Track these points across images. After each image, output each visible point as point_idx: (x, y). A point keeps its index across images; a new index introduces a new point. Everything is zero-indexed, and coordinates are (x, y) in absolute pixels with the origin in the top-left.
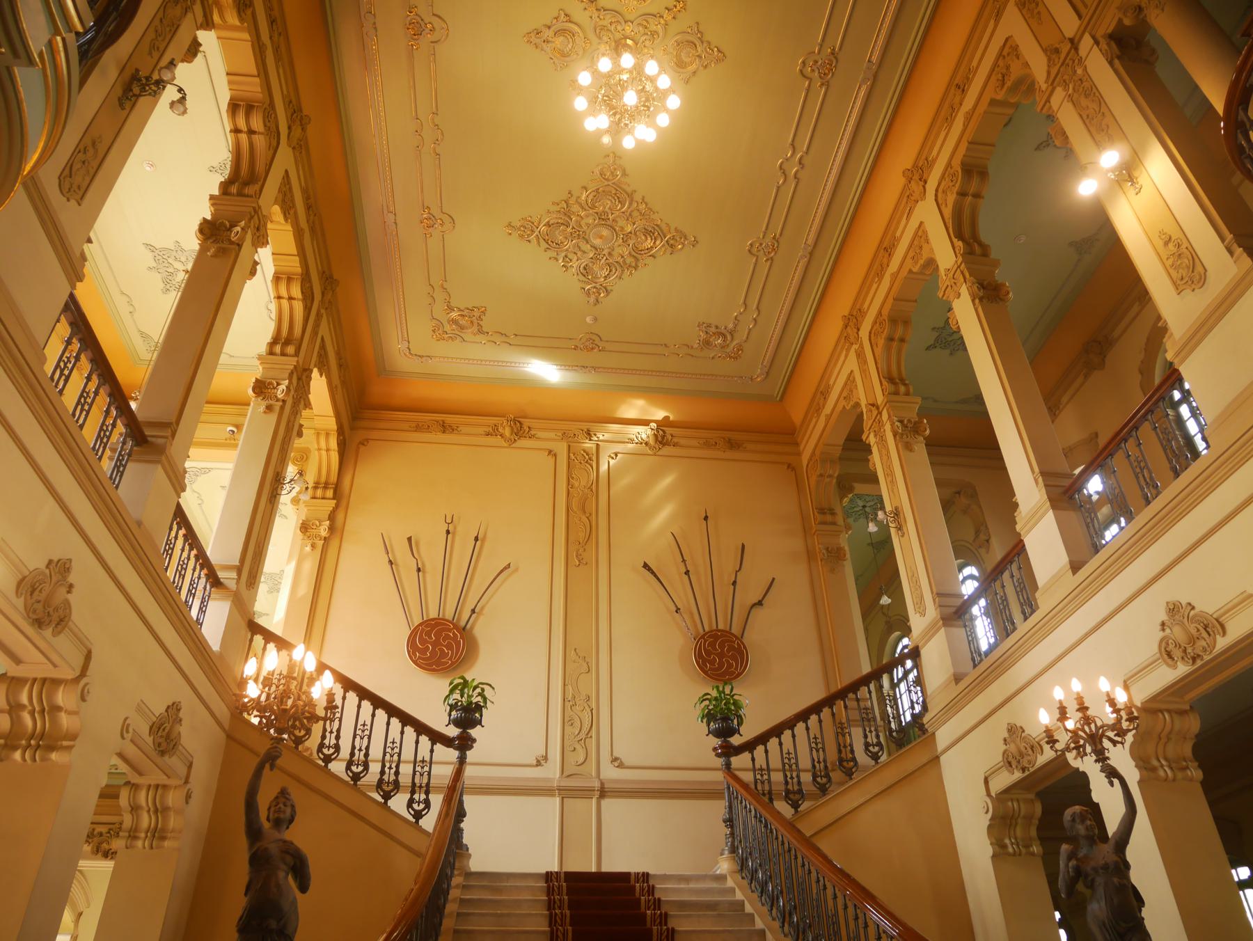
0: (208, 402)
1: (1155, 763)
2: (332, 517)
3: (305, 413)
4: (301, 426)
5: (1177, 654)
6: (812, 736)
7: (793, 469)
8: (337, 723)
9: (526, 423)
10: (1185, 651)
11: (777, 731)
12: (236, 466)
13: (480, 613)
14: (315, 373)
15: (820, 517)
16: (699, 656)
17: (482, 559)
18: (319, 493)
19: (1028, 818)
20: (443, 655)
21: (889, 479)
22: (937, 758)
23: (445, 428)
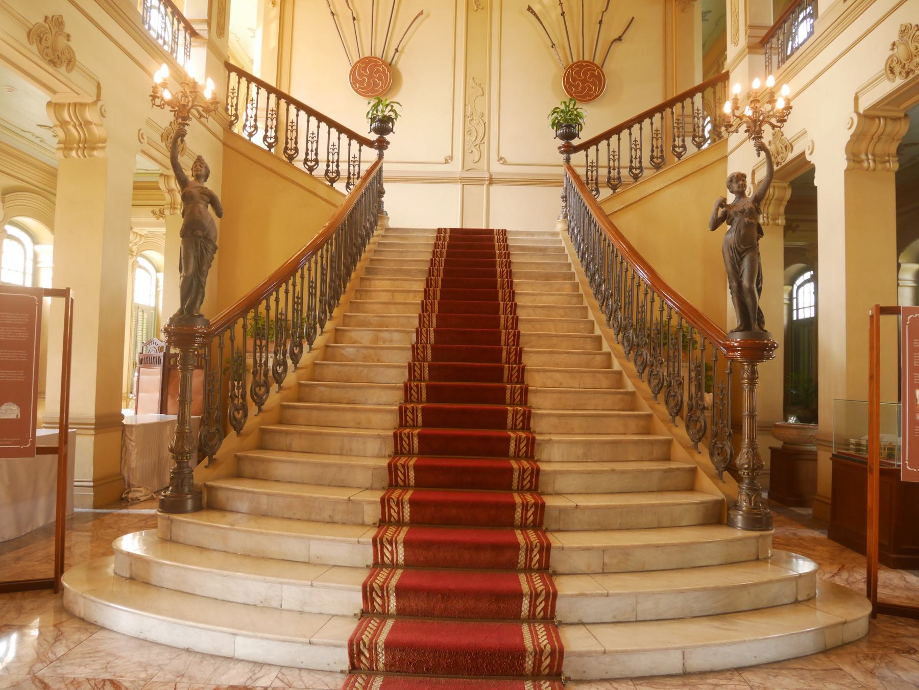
1: (863, 157)
5: (897, 69)
8: (294, 132)
10: (903, 67)
11: (607, 136)
13: (402, 52)
16: (567, 82)
17: (401, 11)
19: (780, 200)
20: (376, 85)
22: (726, 157)
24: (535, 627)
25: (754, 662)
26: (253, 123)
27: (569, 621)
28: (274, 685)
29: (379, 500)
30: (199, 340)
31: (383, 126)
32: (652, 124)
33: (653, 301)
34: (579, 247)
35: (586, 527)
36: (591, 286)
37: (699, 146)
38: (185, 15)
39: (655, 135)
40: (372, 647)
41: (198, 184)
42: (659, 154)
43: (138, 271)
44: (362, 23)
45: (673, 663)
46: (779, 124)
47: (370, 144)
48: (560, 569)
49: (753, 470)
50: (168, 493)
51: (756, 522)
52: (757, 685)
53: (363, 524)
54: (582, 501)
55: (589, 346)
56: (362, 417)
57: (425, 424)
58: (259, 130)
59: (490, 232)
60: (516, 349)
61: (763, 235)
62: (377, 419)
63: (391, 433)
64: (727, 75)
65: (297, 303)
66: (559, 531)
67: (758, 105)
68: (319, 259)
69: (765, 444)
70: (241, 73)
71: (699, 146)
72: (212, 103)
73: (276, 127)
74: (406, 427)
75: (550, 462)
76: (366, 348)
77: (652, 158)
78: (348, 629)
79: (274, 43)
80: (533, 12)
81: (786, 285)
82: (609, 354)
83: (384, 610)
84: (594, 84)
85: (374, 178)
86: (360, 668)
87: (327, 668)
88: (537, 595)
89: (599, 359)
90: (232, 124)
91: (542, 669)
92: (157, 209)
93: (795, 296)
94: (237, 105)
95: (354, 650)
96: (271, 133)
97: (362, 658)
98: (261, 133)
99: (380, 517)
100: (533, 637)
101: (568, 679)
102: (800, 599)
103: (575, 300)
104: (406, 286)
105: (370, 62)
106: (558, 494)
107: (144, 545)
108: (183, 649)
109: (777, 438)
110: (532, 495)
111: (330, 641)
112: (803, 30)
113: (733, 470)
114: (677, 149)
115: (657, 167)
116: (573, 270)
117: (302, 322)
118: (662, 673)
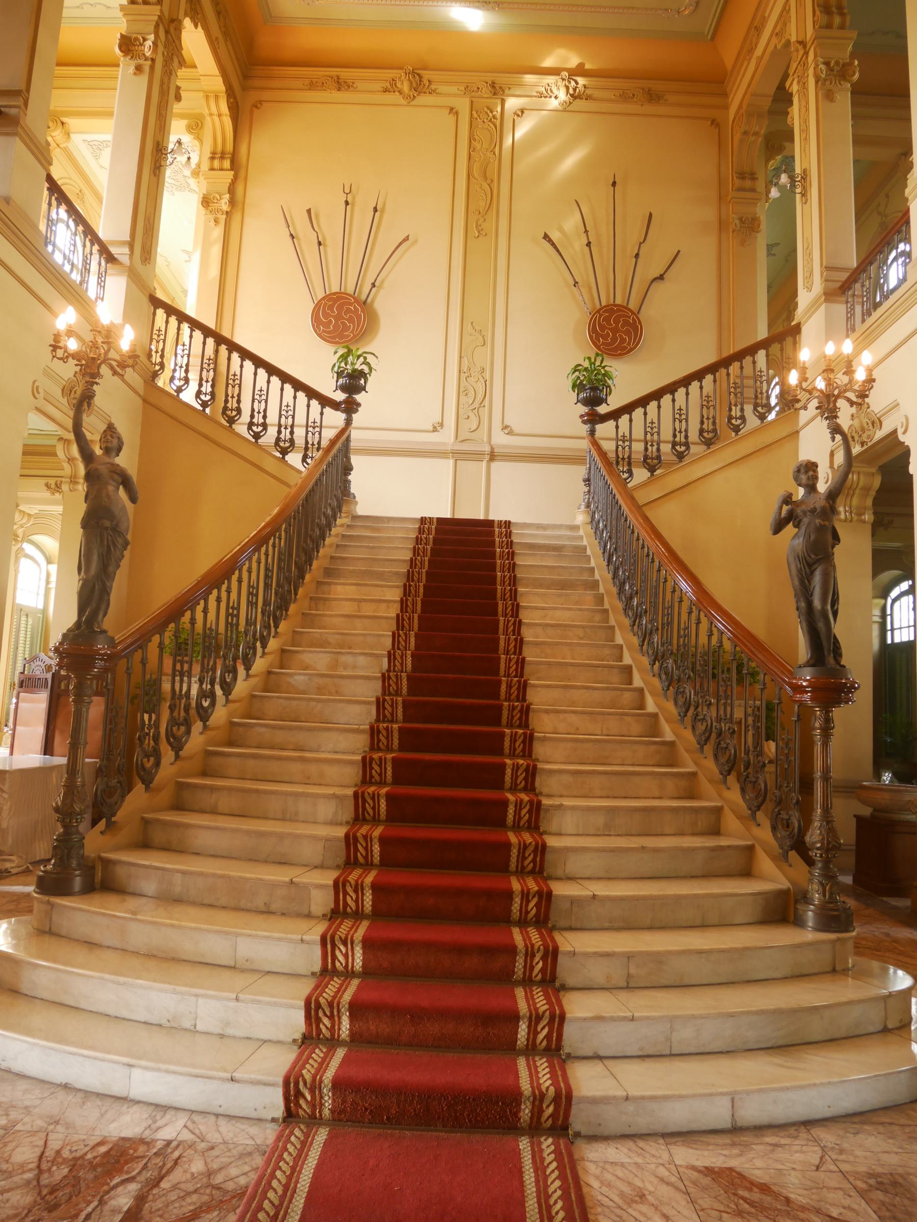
0: (58, 64)
2: (232, 190)
3: (182, 73)
4: (178, 88)
6: (677, 407)
7: (718, 125)
9: (426, 75)
11: (643, 402)
12: (114, 138)
13: (380, 287)
14: (187, 23)
15: (738, 182)
18: (216, 163)
19: (866, 489)
20: (346, 328)
21: (803, 136)
22: (797, 432)
23: (340, 85)
24: (534, 1061)
25: (828, 1113)
26: (183, 374)
27: (579, 1053)
28: (180, 1138)
29: (331, 883)
30: (99, 663)
31: (353, 382)
32: (701, 387)
33: (698, 622)
34: (605, 546)
35: (607, 925)
36: (620, 599)
37: (762, 417)
38: (101, 235)
39: (706, 402)
40: (315, 1087)
41: (107, 460)
42: (711, 427)
43: (24, 562)
44: (329, 250)
45: (717, 1113)
46: (860, 401)
47: (335, 405)
48: (571, 981)
49: (828, 850)
50: (49, 867)
51: (834, 920)
52: (830, 1145)
53: (309, 916)
54: (601, 889)
55: (616, 678)
56: (313, 769)
57: (396, 781)
58: (191, 382)
59: (489, 523)
60: (519, 682)
61: (839, 541)
62: (332, 772)
63: (350, 792)
64: (797, 329)
65: (232, 615)
66: (571, 929)
67: (832, 376)
68: (263, 557)
69: (846, 813)
70: (171, 311)
71: (762, 417)
72: (130, 357)
73: (213, 380)
74: (371, 783)
75: (560, 834)
76: (323, 676)
77: (701, 431)
78: (284, 1059)
79: (214, 271)
80: (550, 241)
81: (874, 598)
82: (641, 691)
83: (333, 1035)
84: (628, 333)
85: (339, 451)
86: (298, 1115)
87: (254, 1115)
88: (539, 1018)
89: (627, 697)
90: (155, 375)
91: (543, 1119)
92: (52, 482)
93: (889, 612)
94: (163, 350)
95: (291, 1090)
96: (207, 388)
97: (302, 1102)
98: (193, 386)
99: (332, 906)
100: (531, 1076)
101: (578, 1135)
102: (890, 1026)
103: (598, 617)
104: (377, 594)
105: (339, 298)
106: (570, 879)
107: (13, 938)
108: (60, 1085)
109: (865, 803)
110: (535, 880)
111: (259, 1077)
112: (894, 274)
113: (801, 847)
114: (733, 421)
115: (708, 443)
116: (597, 576)
117: (237, 640)
118: (704, 1128)
